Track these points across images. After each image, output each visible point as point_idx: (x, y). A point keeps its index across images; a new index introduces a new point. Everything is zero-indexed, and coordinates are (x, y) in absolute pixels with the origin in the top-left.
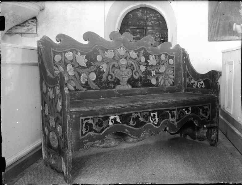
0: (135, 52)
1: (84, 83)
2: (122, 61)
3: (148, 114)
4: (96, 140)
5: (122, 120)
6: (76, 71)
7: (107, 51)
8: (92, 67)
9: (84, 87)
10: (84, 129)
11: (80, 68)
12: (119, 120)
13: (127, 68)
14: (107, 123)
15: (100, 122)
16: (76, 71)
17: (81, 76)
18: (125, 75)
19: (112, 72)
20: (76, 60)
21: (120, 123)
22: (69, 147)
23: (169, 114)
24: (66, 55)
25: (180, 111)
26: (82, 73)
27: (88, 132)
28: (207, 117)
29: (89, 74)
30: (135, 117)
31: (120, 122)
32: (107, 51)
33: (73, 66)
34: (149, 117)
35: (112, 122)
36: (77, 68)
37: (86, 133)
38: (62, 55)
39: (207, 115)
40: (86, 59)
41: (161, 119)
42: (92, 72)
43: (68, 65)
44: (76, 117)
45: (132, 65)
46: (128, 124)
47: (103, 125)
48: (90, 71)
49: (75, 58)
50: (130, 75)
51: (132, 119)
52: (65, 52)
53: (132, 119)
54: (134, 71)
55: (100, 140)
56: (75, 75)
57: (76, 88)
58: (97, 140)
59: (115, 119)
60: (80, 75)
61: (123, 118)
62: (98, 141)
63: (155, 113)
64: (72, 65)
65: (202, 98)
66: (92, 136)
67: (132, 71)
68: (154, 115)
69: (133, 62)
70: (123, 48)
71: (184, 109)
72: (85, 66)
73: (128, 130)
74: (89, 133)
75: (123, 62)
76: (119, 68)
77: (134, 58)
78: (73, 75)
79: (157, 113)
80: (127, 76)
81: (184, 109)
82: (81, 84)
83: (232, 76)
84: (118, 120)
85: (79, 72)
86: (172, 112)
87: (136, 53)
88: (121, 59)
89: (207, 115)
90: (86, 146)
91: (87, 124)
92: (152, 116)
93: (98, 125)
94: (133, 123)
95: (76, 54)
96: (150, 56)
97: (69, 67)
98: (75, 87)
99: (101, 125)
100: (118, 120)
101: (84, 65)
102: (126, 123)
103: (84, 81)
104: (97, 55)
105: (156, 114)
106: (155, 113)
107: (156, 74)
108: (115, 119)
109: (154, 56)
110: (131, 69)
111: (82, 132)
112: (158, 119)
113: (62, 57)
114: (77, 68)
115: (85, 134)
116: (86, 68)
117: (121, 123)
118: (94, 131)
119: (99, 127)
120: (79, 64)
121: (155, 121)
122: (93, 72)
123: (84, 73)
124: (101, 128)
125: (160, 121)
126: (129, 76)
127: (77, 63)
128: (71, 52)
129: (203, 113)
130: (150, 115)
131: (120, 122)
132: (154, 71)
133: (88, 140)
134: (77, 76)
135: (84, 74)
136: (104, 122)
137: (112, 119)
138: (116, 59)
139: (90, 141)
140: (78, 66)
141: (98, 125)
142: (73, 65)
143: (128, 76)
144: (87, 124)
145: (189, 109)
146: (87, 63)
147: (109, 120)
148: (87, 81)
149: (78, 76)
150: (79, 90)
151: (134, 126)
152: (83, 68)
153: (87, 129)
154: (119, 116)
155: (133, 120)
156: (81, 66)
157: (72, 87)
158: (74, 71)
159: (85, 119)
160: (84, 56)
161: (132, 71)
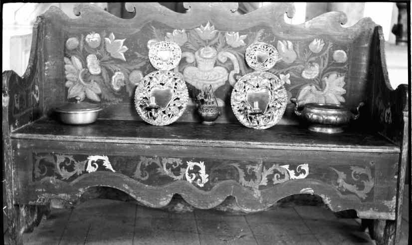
0: (240, 34)
1: (117, 89)
2: (205, 52)
3: (179, 162)
4: (61, 193)
5: (117, 165)
6: (103, 66)
7: (171, 32)
8: (136, 61)
9: (116, 96)
10: (37, 170)
11: (113, 61)
12: (110, 165)
13: (215, 65)
14: (84, 166)
15: (68, 163)
16: (103, 66)
17: (114, 77)
18: (209, 79)
19: (180, 72)
20: (105, 47)
21: (111, 171)
22: (8, 194)
23: (240, 171)
24: (87, 39)
25: (271, 169)
26: (115, 71)
27: (45, 176)
28: (362, 194)
29: (129, 74)
30: (147, 165)
31: (112, 169)
32: (171, 32)
33: (99, 58)
34: (182, 170)
35: (93, 165)
36: (107, 61)
37: (41, 177)
38: (79, 39)
39: (361, 187)
40: (125, 47)
41: (217, 178)
42: (135, 69)
43: (89, 55)
44: (21, 148)
45: (229, 60)
46: (131, 175)
47: (75, 168)
48: (132, 68)
49: (103, 44)
50: (221, 80)
51: (139, 168)
52: (85, 35)
53: (139, 168)
54: (232, 73)
55: (68, 194)
56: (100, 75)
57: (102, 97)
58: (63, 193)
59: (100, 162)
60: (111, 74)
61: (118, 162)
62: (63, 195)
63: (198, 164)
64: (98, 58)
65: (322, 156)
66: (53, 185)
67: (229, 72)
68: (196, 169)
69: (232, 53)
70: (211, 25)
71: (287, 167)
72: (123, 58)
73: (129, 186)
74: (46, 178)
75: (207, 54)
76: (197, 66)
77: (236, 47)
78: (98, 73)
79: (204, 164)
80: (215, 80)
81: (287, 167)
82: (112, 91)
83: (360, 162)
84: (107, 164)
85: (110, 68)
86: (249, 167)
87: (242, 36)
88: (204, 47)
89: (361, 187)
90: (42, 199)
91: (42, 161)
92: (192, 169)
93: (63, 167)
94: (142, 176)
95: (107, 36)
96: (280, 42)
97: (91, 59)
98: (100, 95)
99: (70, 169)
100: (107, 164)
101: (119, 57)
102: (124, 172)
103: (118, 86)
104: (149, 39)
105: (202, 165)
106: (198, 164)
107: (291, 80)
108: (100, 162)
109: (290, 43)
110: (227, 70)
111: (34, 175)
112: (208, 178)
113: (80, 43)
114: (107, 61)
115: (39, 179)
116: (125, 62)
117: (114, 171)
118: (56, 177)
119: (67, 172)
120: (110, 55)
121: (199, 180)
122: (139, 69)
123: (119, 71)
124: (72, 174)
125: (212, 180)
126: (220, 82)
127: (107, 53)
128: (97, 34)
129: (348, 181)
130: (185, 166)
131: (112, 169)
132: (288, 75)
133: (44, 190)
134: (105, 76)
135: (120, 73)
136: (77, 164)
137: (93, 162)
138: (190, 46)
139: (49, 192)
140: (108, 57)
141: (63, 167)
142: (99, 57)
143: (217, 82)
144: (42, 161)
145: (300, 168)
146: (126, 54)
147: (87, 162)
148: (125, 86)
149: (108, 76)
150: (106, 99)
151: (143, 182)
152: (119, 61)
153: (43, 171)
154: (111, 159)
155: (141, 169)
156: (113, 59)
157: (94, 94)
158: (101, 66)
159: (39, 155)
160: (122, 41)
161: (229, 72)
